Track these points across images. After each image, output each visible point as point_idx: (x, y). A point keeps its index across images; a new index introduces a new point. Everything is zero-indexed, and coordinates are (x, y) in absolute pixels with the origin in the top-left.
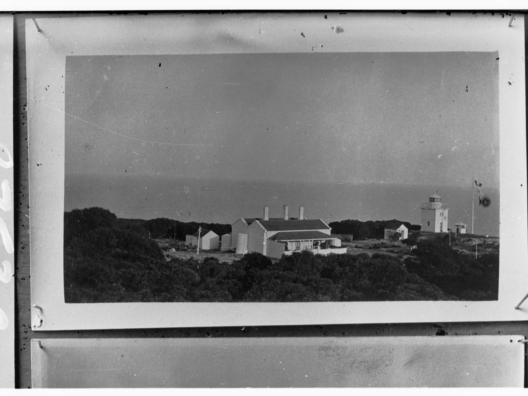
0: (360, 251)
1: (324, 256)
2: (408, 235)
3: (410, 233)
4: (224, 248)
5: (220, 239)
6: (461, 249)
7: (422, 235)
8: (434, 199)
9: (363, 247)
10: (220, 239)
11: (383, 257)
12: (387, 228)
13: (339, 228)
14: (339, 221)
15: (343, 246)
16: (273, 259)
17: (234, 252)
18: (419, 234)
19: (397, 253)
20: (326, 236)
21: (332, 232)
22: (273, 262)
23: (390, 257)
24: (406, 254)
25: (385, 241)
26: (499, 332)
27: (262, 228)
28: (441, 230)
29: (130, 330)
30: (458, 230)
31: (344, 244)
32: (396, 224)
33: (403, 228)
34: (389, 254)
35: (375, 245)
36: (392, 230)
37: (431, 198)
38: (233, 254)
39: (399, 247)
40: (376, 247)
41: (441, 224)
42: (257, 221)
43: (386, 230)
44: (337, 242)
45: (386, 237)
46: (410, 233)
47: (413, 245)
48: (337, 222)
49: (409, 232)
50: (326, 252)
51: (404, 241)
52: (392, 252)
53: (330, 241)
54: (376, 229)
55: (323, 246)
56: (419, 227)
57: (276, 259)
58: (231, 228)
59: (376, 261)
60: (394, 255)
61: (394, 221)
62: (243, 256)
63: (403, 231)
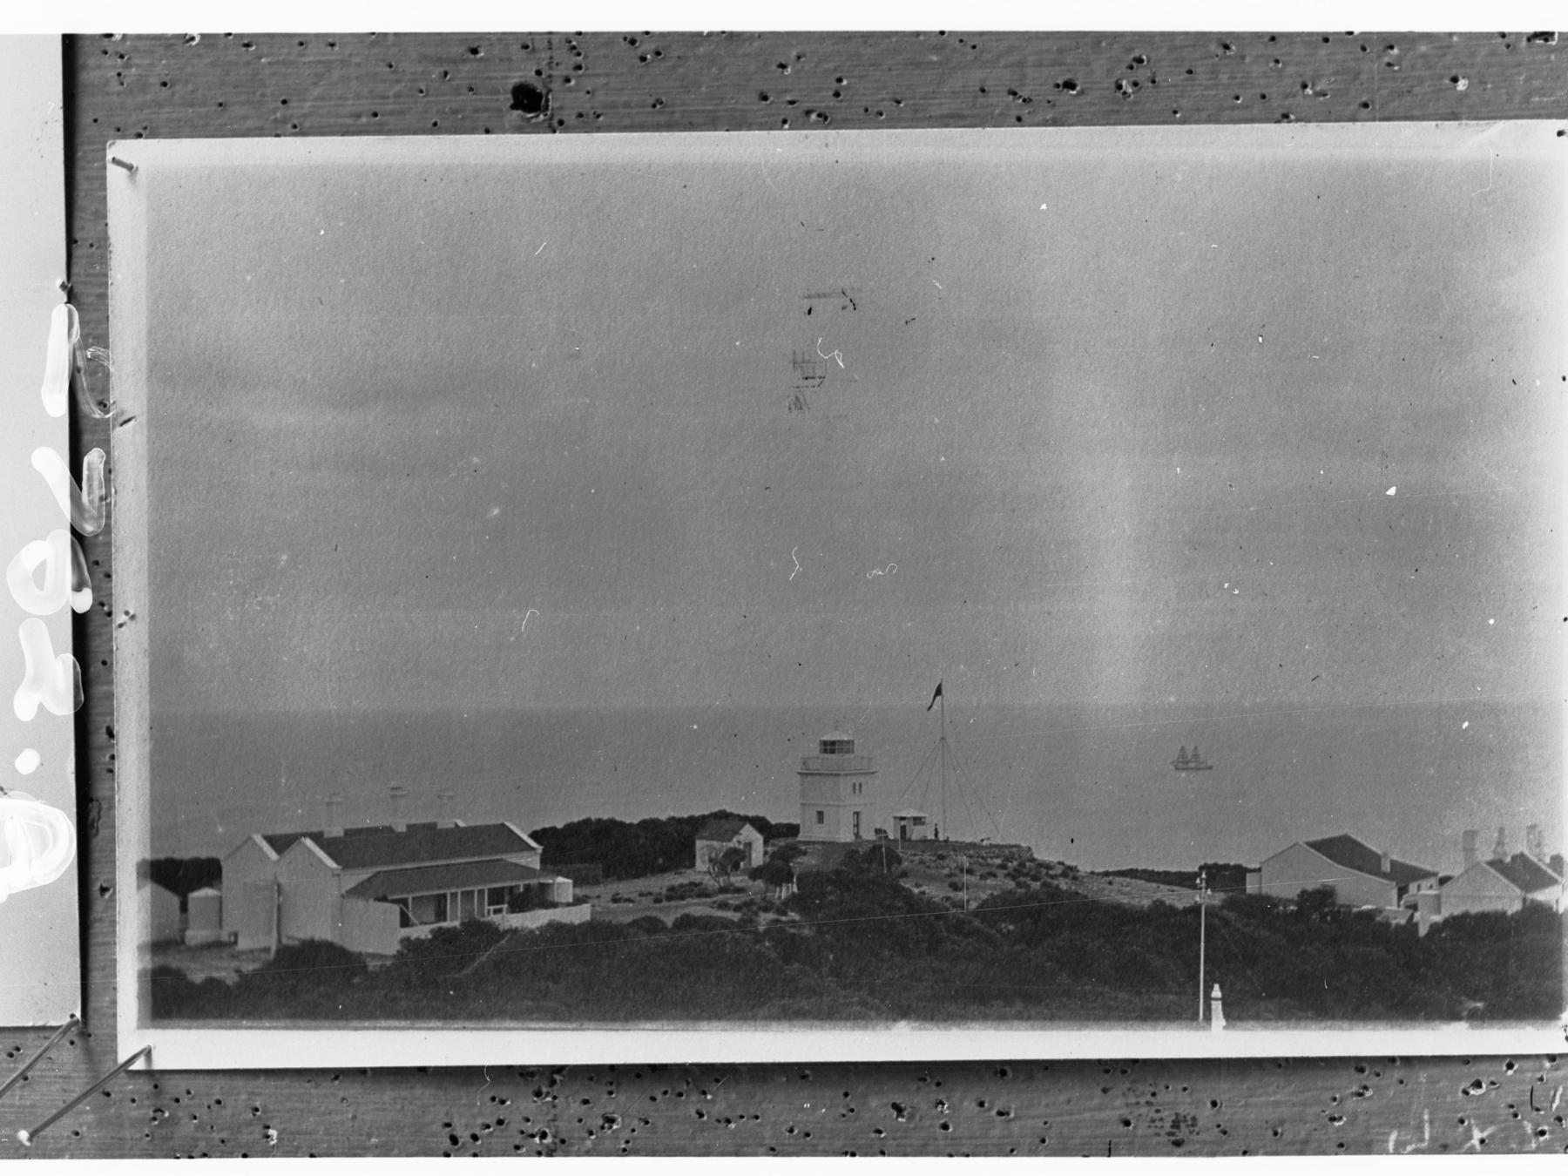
0: (646, 908)
1: (531, 931)
2: (766, 853)
3: (770, 849)
4: (197, 935)
5: (184, 908)
6: (917, 885)
7: (805, 853)
8: (833, 743)
9: (628, 899)
10: (184, 908)
11: (706, 923)
12: (701, 838)
13: (562, 846)
14: (560, 826)
15: (578, 901)
16: (374, 956)
17: (183, 942)
18: (795, 851)
19: (737, 909)
20: (527, 871)
21: (543, 861)
22: (372, 965)
23: (726, 924)
24: (766, 910)
25: (696, 878)
26: (1019, 119)
27: (320, 861)
28: (857, 835)
29: (469, 1068)
30: (903, 829)
31: (580, 892)
32: (724, 822)
33: (749, 833)
34: (720, 913)
35: (672, 889)
36: (715, 844)
37: (825, 743)
38: (226, 953)
39: (739, 890)
40: (675, 894)
41: (1123, 995)
42: (308, 842)
43: (699, 844)
44: (564, 886)
45: (701, 864)
46: (770, 849)
47: (1474, 1000)
48: (554, 829)
49: (766, 842)
50: (534, 920)
51: (755, 874)
52: (723, 906)
53: (544, 888)
54: (667, 844)
55: (521, 902)
56: (793, 830)
57: (381, 957)
58: (220, 868)
59: (690, 936)
60: (735, 916)
61: (722, 816)
62: (272, 955)
63: (749, 845)
